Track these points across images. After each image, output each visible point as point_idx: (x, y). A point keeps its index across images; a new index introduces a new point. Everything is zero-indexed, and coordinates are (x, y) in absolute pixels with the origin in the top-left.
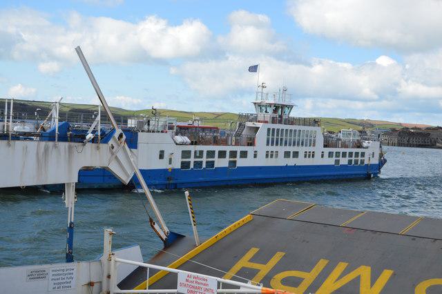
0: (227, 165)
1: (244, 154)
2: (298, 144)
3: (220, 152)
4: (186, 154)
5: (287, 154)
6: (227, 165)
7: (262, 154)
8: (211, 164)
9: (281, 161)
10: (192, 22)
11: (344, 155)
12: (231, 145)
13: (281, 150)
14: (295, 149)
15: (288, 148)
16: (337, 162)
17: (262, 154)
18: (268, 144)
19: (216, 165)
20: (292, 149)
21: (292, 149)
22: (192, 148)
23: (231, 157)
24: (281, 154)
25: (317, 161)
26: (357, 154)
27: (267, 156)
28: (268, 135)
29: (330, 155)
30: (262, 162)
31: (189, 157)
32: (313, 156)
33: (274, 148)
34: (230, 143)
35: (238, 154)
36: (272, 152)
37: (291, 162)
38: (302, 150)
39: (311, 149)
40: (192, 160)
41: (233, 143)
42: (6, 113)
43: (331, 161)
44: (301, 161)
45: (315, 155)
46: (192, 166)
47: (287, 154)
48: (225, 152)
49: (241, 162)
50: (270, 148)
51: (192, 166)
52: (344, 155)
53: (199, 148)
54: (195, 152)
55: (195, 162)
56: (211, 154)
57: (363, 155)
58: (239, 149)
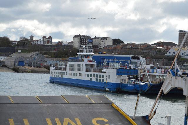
48: (77, 74)
49: (64, 76)
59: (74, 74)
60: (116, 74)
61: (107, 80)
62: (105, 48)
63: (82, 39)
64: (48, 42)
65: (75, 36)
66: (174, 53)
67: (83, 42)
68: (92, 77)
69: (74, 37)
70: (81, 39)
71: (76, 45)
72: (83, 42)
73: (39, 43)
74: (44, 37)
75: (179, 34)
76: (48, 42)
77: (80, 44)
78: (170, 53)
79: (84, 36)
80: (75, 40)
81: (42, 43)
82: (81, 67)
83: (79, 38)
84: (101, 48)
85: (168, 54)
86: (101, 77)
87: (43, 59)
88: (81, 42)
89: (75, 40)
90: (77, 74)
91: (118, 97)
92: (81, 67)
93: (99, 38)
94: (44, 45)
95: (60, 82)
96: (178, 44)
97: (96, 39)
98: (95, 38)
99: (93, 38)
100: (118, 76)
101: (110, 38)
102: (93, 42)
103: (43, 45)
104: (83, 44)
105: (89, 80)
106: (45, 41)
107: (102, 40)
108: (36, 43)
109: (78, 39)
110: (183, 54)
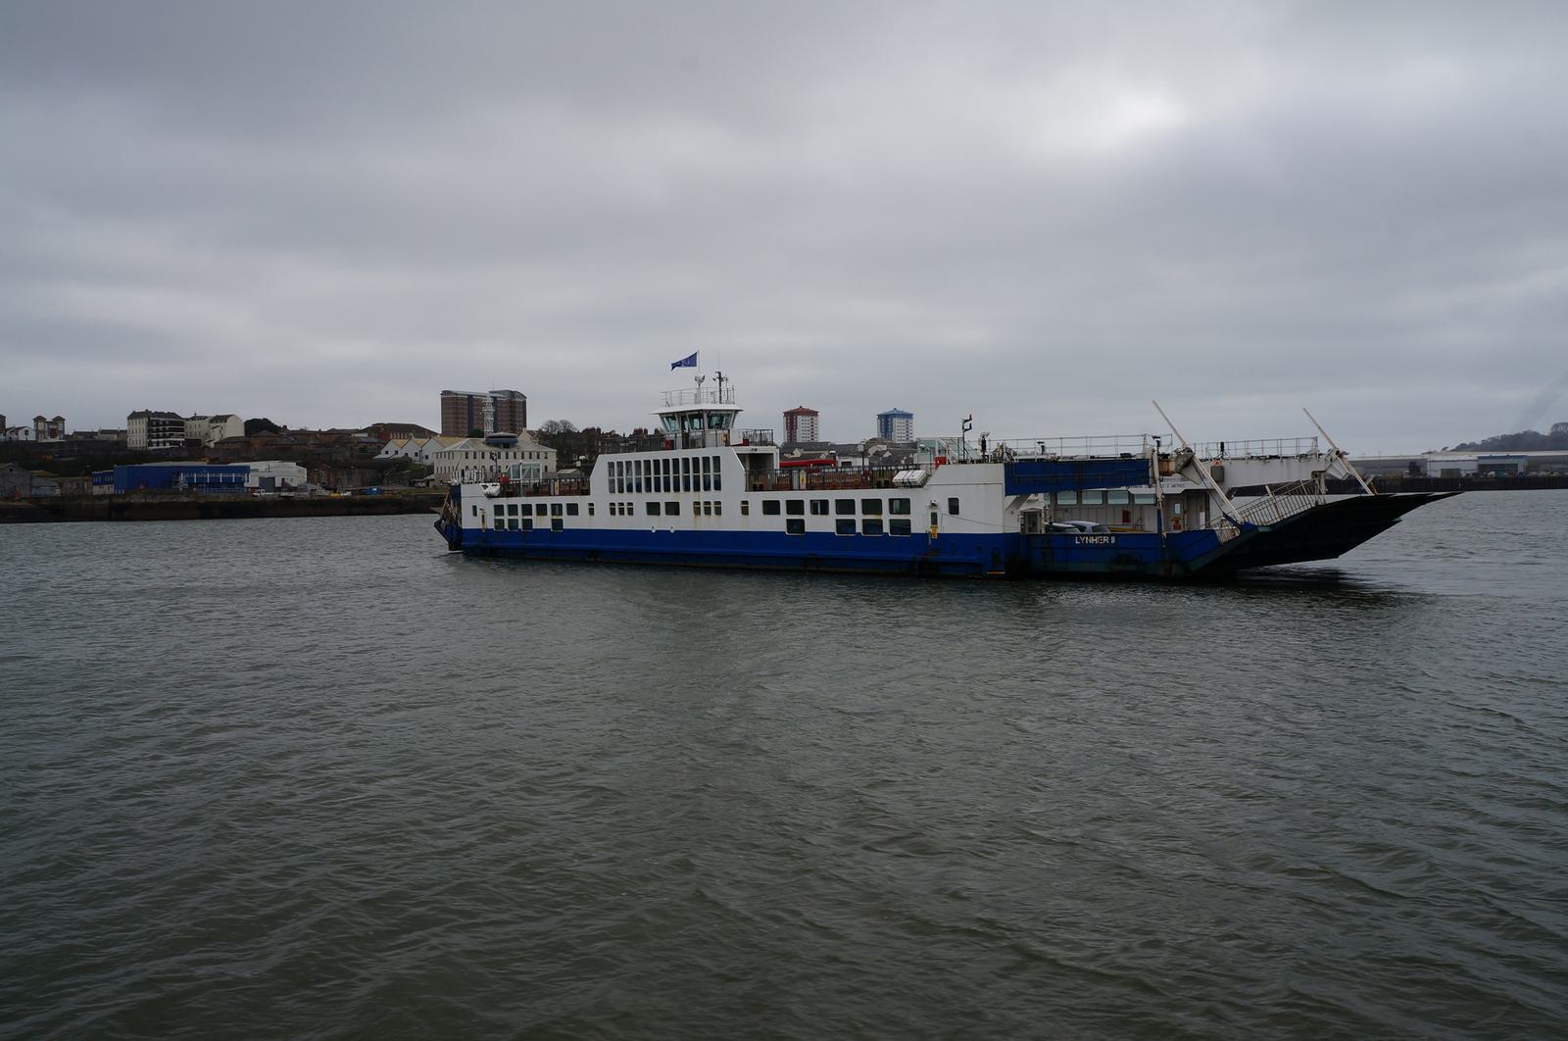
0: (783, 528)
1: (573, 509)
2: (630, 489)
3: (839, 503)
4: (499, 510)
5: (653, 509)
6: (783, 528)
7: (602, 509)
8: (528, 523)
9: (641, 522)
11: (542, 510)
12: (555, 495)
13: (640, 500)
14: (671, 497)
15: (654, 497)
16: (796, 526)
17: (602, 509)
18: (612, 491)
20: (663, 498)
22: (505, 502)
23: (553, 514)
24: (640, 508)
25: (730, 521)
26: (871, 506)
27: (613, 512)
28: (611, 474)
29: (771, 508)
30: (603, 521)
33: (625, 498)
34: (795, 485)
35: (807, 507)
36: (706, 503)
37: (664, 523)
38: (686, 499)
39: (711, 496)
41: (557, 493)
43: (778, 523)
44: (686, 521)
45: (471, 512)
47: (653, 509)
48: (825, 504)
49: (570, 522)
50: (617, 498)
51: (859, 529)
52: (542, 510)
53: (513, 501)
54: (891, 501)
55: (864, 521)
56: (527, 509)
57: (904, 506)
58: (565, 500)
59: (814, 504)
60: (1001, 488)
61: (483, 522)
62: (221, 446)
63: (154, 423)
64: (53, 433)
65: (134, 416)
66: (397, 452)
67: (158, 431)
68: (534, 517)
69: (129, 418)
70: (150, 423)
71: (138, 438)
72: (158, 431)
73: (22, 437)
74: (39, 419)
75: (442, 399)
76: (53, 433)
77: (150, 437)
78: (387, 453)
79: (161, 414)
80: (134, 427)
81: (32, 437)
82: (621, 474)
83: (145, 420)
84: (208, 447)
85: (383, 456)
86: (865, 512)
87: (28, 481)
88: (149, 431)
89: (134, 427)
90: (673, 509)
91: (493, 565)
92: (621, 474)
93: (205, 418)
94: (40, 441)
95: (1320, 571)
96: (438, 429)
97: (197, 422)
98: (193, 419)
99: (187, 419)
100: (1013, 498)
101: (236, 417)
102: (187, 430)
103: (34, 444)
104: (158, 437)
105: (549, 526)
106: (43, 432)
107: (214, 425)
108: (14, 437)
109: (142, 425)
110: (416, 454)
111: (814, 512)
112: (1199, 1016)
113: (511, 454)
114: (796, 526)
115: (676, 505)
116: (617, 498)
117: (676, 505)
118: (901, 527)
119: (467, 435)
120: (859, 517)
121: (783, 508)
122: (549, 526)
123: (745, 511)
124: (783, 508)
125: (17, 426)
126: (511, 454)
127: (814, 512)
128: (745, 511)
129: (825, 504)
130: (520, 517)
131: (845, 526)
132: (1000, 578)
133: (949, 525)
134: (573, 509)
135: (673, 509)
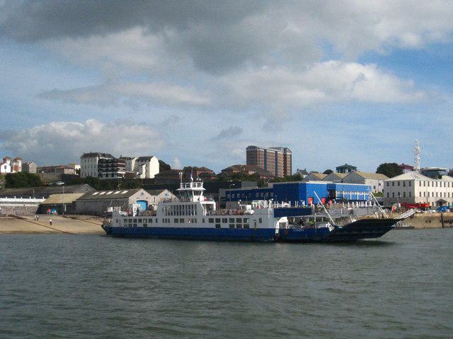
0: (215, 227)
1: (151, 221)
3: (216, 219)
5: (176, 221)
6: (215, 227)
7: (160, 221)
9: (172, 225)
10: (377, 68)
11: (225, 221)
13: (172, 218)
15: (176, 217)
16: (218, 226)
17: (160, 221)
19: (222, 227)
20: (179, 217)
21: (179, 217)
26: (239, 220)
27: (163, 221)
29: (211, 221)
30: (160, 225)
31: (241, 222)
32: (196, 221)
33: (167, 217)
37: (179, 225)
40: (243, 224)
42: (22, 205)
43: (213, 225)
46: (243, 227)
47: (182, 221)
48: (226, 219)
49: (149, 225)
90: (176, 221)
111: (223, 222)
112: (363, 60)
113: (439, 196)
114: (218, 226)
115: (183, 220)
116: (165, 217)
117: (183, 220)
118: (247, 226)
119: (77, 204)
120: (235, 223)
121: (215, 221)
122: (228, 227)
123: (204, 221)
124: (215, 221)
125: (399, 164)
126: (439, 196)
127: (223, 222)
128: (204, 221)
129: (226, 219)
130: (235, 223)
131: (232, 226)
132: (273, 242)
133: (259, 226)
134: (151, 221)
135: (182, 221)
